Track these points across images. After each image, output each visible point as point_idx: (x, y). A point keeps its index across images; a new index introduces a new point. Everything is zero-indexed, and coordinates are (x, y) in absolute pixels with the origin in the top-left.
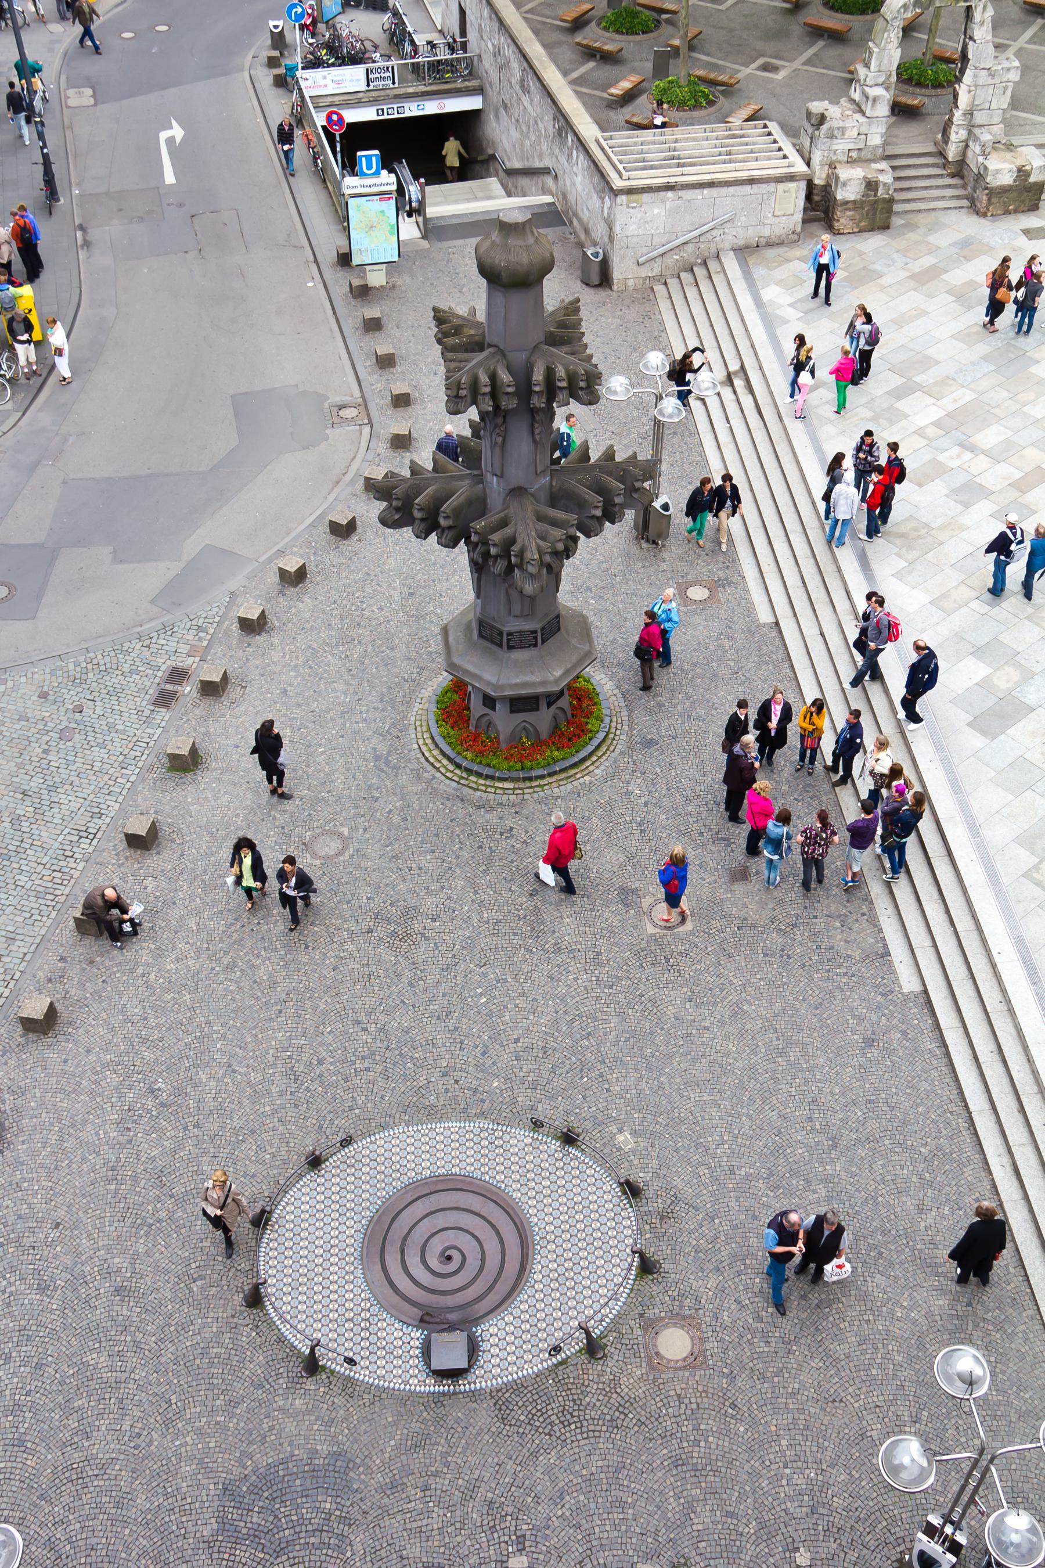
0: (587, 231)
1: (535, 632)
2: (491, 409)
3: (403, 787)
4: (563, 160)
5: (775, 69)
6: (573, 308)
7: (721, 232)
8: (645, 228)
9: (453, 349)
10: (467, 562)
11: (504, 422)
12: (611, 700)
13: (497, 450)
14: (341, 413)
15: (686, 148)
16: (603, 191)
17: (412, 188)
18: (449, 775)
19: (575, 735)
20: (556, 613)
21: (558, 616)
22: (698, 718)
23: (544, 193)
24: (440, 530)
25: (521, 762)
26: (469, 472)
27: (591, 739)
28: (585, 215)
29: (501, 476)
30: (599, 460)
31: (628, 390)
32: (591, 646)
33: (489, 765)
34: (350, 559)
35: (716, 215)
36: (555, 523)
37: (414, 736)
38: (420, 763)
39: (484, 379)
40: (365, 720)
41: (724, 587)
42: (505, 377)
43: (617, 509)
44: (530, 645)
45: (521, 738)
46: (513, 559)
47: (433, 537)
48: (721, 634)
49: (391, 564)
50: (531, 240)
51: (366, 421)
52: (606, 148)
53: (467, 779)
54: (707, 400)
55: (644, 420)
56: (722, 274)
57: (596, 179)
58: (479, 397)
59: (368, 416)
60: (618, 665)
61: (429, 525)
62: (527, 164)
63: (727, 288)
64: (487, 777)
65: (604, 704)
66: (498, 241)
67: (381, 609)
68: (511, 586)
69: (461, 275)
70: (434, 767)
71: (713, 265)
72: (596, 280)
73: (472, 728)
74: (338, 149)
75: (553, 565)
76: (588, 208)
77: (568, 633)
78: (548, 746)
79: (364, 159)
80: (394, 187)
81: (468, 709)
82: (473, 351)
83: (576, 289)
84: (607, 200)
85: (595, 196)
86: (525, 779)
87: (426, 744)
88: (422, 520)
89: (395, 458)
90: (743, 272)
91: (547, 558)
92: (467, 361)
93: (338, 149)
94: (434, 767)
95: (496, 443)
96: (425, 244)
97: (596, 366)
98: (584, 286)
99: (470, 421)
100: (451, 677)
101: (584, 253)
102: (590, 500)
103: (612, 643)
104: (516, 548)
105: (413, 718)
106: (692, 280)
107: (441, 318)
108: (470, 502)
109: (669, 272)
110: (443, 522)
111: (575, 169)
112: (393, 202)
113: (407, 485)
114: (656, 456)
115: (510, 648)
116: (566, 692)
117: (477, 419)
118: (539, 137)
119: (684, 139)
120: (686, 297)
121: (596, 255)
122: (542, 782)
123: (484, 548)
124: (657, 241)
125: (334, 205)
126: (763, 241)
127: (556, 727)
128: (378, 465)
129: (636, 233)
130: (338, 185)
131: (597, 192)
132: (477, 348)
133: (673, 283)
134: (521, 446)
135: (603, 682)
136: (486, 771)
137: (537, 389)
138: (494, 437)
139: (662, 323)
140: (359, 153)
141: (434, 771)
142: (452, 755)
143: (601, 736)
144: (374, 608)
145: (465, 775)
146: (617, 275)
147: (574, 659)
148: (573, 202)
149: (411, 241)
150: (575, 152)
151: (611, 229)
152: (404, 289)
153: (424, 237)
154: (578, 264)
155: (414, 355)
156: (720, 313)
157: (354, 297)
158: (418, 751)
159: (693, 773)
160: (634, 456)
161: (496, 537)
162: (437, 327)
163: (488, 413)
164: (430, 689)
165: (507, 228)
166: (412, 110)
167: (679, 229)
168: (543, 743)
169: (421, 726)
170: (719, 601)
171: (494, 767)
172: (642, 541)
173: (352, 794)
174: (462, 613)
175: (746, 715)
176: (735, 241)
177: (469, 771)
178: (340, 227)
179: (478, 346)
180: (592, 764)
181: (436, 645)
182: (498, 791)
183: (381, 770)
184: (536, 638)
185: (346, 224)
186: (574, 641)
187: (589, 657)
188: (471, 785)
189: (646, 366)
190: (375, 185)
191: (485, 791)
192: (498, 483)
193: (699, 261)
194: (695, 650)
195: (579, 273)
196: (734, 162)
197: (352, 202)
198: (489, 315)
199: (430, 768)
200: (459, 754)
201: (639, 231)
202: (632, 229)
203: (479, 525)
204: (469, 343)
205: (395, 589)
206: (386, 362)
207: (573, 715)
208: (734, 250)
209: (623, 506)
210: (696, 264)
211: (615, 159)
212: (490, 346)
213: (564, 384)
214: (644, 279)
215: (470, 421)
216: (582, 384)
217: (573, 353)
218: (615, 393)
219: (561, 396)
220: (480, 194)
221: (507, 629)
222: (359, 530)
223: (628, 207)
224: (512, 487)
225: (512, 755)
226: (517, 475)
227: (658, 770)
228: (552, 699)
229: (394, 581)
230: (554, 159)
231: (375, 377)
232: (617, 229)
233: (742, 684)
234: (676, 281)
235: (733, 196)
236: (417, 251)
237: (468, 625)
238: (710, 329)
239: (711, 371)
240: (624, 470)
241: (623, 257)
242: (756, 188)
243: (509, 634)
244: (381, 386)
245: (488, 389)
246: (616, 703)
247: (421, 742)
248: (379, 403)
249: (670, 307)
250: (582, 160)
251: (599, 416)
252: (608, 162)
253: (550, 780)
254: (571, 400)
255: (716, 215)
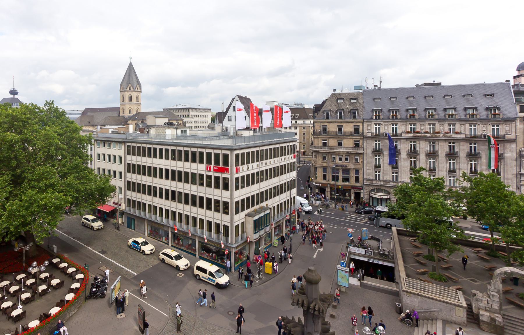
5: (476, 282)
96: (360, 287)
166: (376, 262)
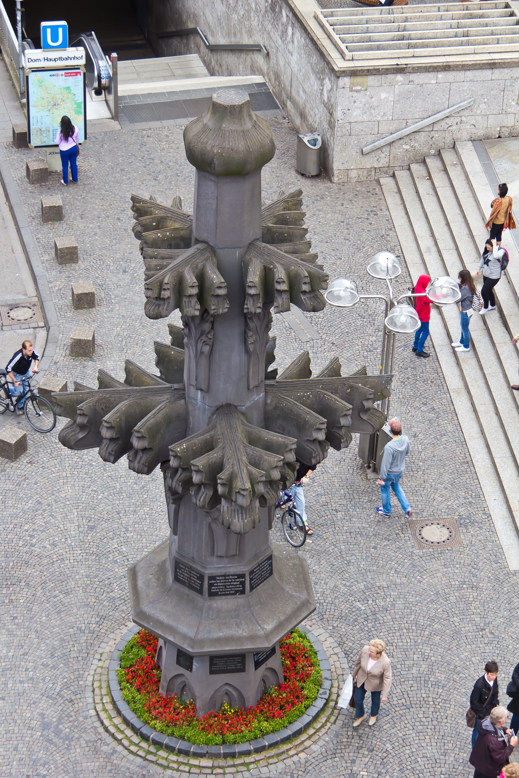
0: (303, 116)
1: (242, 576)
2: (197, 313)
3: (76, 763)
4: (276, 36)
6: (295, 201)
7: (458, 120)
8: (371, 114)
9: (155, 244)
10: (162, 488)
11: (212, 328)
12: (331, 661)
13: (204, 361)
14: (12, 314)
15: (417, 28)
16: (323, 72)
17: (102, 63)
18: (133, 748)
19: (288, 703)
20: (267, 554)
21: (270, 558)
22: (437, 684)
23: (253, 73)
24: (132, 453)
25: (222, 734)
26: (168, 385)
27: (306, 708)
28: (301, 98)
29: (207, 391)
30: (322, 374)
31: (353, 296)
32: (309, 594)
33: (182, 738)
34: (19, 485)
35: (452, 101)
36: (269, 447)
37: (90, 700)
38: (97, 733)
39: (191, 279)
40: (32, 679)
41: (466, 527)
42: (215, 277)
43: (343, 432)
44: (236, 592)
45: (222, 705)
46: (220, 489)
47: (124, 460)
48: (464, 583)
49: (68, 491)
50: (249, 125)
51: (42, 324)
52: (327, 25)
53: (155, 755)
54: (444, 309)
55: (370, 330)
56: (459, 167)
57: (315, 58)
58: (185, 299)
59: (45, 317)
60: (340, 617)
61: (120, 446)
62: (233, 41)
63: (465, 183)
64: (180, 752)
65: (323, 666)
66: (211, 124)
67: (54, 545)
68: (215, 520)
69: (156, 161)
70: (116, 739)
71: (448, 157)
72: (313, 170)
73: (162, 692)
74: (19, 18)
75: (267, 496)
76: (304, 91)
77: (281, 577)
78: (255, 715)
79: (49, 31)
80: (83, 62)
81: (158, 668)
82: (178, 247)
83: (294, 183)
84: (327, 81)
85: (313, 77)
86: (226, 756)
87: (106, 710)
88: (111, 440)
89: (75, 367)
90: (484, 165)
91: (261, 488)
92: (171, 258)
93: (19, 18)
94: (116, 739)
95: (202, 353)
96: (115, 125)
97: (321, 267)
98: (299, 177)
99: (171, 327)
100: (138, 629)
101: (300, 140)
102: (312, 421)
103: (333, 591)
104: (223, 476)
105: (90, 678)
106: (425, 173)
107: (140, 209)
108: (169, 420)
109: (397, 164)
110: (136, 443)
111: (290, 47)
112: (81, 78)
113: (96, 398)
114: (386, 372)
115: (212, 594)
116: (278, 649)
117: (180, 324)
118: (248, 11)
119: (415, 17)
120: (417, 192)
121: (314, 142)
122: (248, 759)
123: (185, 475)
124: (384, 129)
125: (11, 79)
126: (505, 132)
127: (265, 692)
128: (55, 375)
129: (360, 119)
130: (16, 57)
131: (316, 73)
132: (182, 244)
133: (402, 175)
134: (231, 355)
135: (322, 638)
136: (179, 745)
137: (252, 291)
138: (200, 345)
139: (390, 220)
140: (43, 24)
141: (114, 744)
142: (137, 723)
143: (320, 703)
144: (46, 544)
145: (152, 749)
146: (337, 164)
147: (289, 610)
148: (287, 84)
149: (99, 122)
150: (290, 29)
151: (331, 114)
152: (90, 174)
153: (115, 117)
154: (293, 152)
155: (101, 249)
156: (458, 211)
157: (32, 182)
158: (95, 719)
159: (431, 751)
160: (363, 371)
161: (200, 462)
162: (136, 218)
163: (193, 318)
164: (111, 643)
165: (221, 111)
167: (410, 116)
168: (248, 711)
169: (100, 687)
170: (461, 543)
171: (189, 740)
172: (369, 471)
173: (13, 771)
174: (154, 552)
175: (496, 681)
176: (474, 130)
177: (157, 744)
178: (17, 104)
179: (184, 242)
180: (309, 738)
181: (122, 588)
182: (193, 770)
183: (50, 741)
184: (243, 583)
185: (24, 101)
186: (288, 588)
187: (306, 608)
188: (161, 761)
189: (374, 267)
190: (60, 59)
191: (178, 770)
192: (203, 398)
193: (433, 152)
194: (432, 601)
195: (294, 162)
196: (472, 45)
197: (33, 77)
198: (198, 207)
199: (109, 740)
200: (146, 723)
201: (363, 116)
202: (356, 114)
203: (180, 447)
204: (173, 238)
205: (71, 521)
206: (67, 256)
207: (285, 678)
208: (473, 141)
209: (351, 429)
210: (429, 155)
211: (336, 37)
212: (197, 241)
213: (284, 287)
214: (369, 170)
215: (171, 327)
216: (305, 288)
217: (294, 252)
218: (339, 298)
219: (280, 300)
220: (179, 72)
221: (208, 572)
222: (31, 450)
223: (351, 90)
224: (219, 404)
225: (211, 726)
226: (225, 390)
227: (389, 746)
228: (261, 658)
229: (71, 512)
230: (266, 36)
231: (54, 273)
232: (338, 114)
233: (490, 643)
234: (406, 173)
235: (472, 81)
236: (105, 133)
237: (162, 567)
238: (446, 228)
239: (448, 275)
240: (351, 387)
241: (345, 146)
242: (497, 73)
243: (212, 578)
244: (62, 284)
245: (195, 291)
246: (338, 664)
247: (99, 707)
248: (57, 304)
249: (399, 202)
250: (299, 37)
251: (316, 324)
252: (328, 41)
253: (257, 757)
254: (292, 304)
255: (452, 101)
